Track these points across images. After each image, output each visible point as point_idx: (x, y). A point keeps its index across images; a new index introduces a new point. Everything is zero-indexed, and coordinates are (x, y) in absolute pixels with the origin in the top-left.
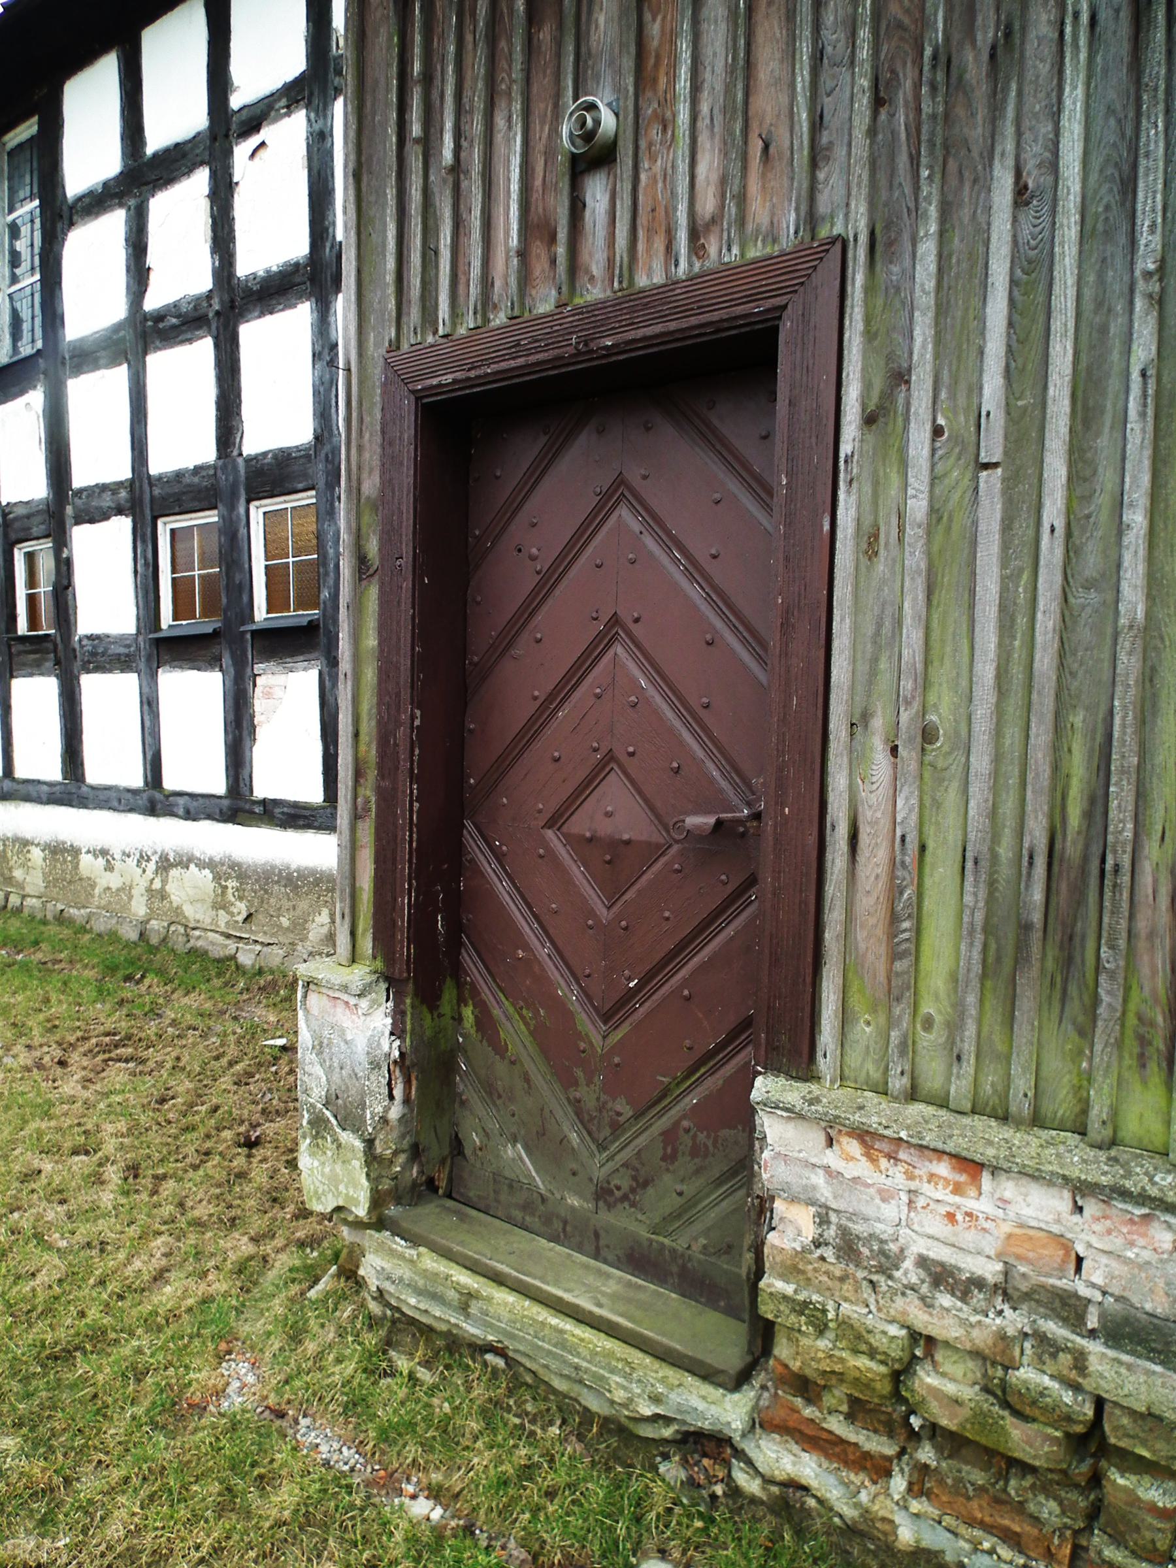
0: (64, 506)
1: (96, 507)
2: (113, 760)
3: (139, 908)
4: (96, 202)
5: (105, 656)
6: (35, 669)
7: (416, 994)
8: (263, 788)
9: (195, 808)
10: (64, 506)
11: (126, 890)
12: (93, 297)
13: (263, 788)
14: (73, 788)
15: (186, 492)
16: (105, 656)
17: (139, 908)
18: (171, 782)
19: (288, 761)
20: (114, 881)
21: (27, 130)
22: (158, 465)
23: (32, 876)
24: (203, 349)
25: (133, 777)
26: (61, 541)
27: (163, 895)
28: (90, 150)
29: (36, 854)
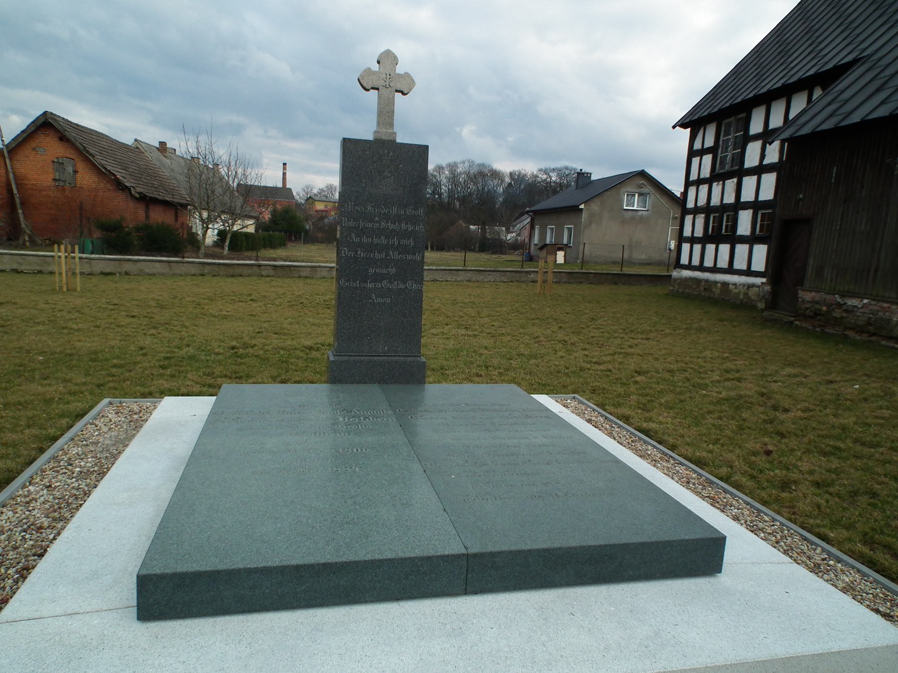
0: (739, 205)
1: (746, 206)
2: (740, 263)
3: (741, 297)
4: (756, 137)
5: (743, 240)
6: (699, 243)
7: (197, 235)
8: (753, 268)
9: (740, 272)
10: (739, 205)
11: (739, 293)
12: (752, 158)
13: (753, 268)
14: (730, 270)
15: (715, 209)
16: (743, 240)
17: (741, 297)
18: (753, 269)
19: (759, 264)
20: (736, 291)
21: (743, 115)
22: (761, 198)
23: (717, 291)
24: (755, 178)
25: (745, 267)
26: (736, 214)
27: (747, 294)
28: (756, 126)
29: (719, 285)
